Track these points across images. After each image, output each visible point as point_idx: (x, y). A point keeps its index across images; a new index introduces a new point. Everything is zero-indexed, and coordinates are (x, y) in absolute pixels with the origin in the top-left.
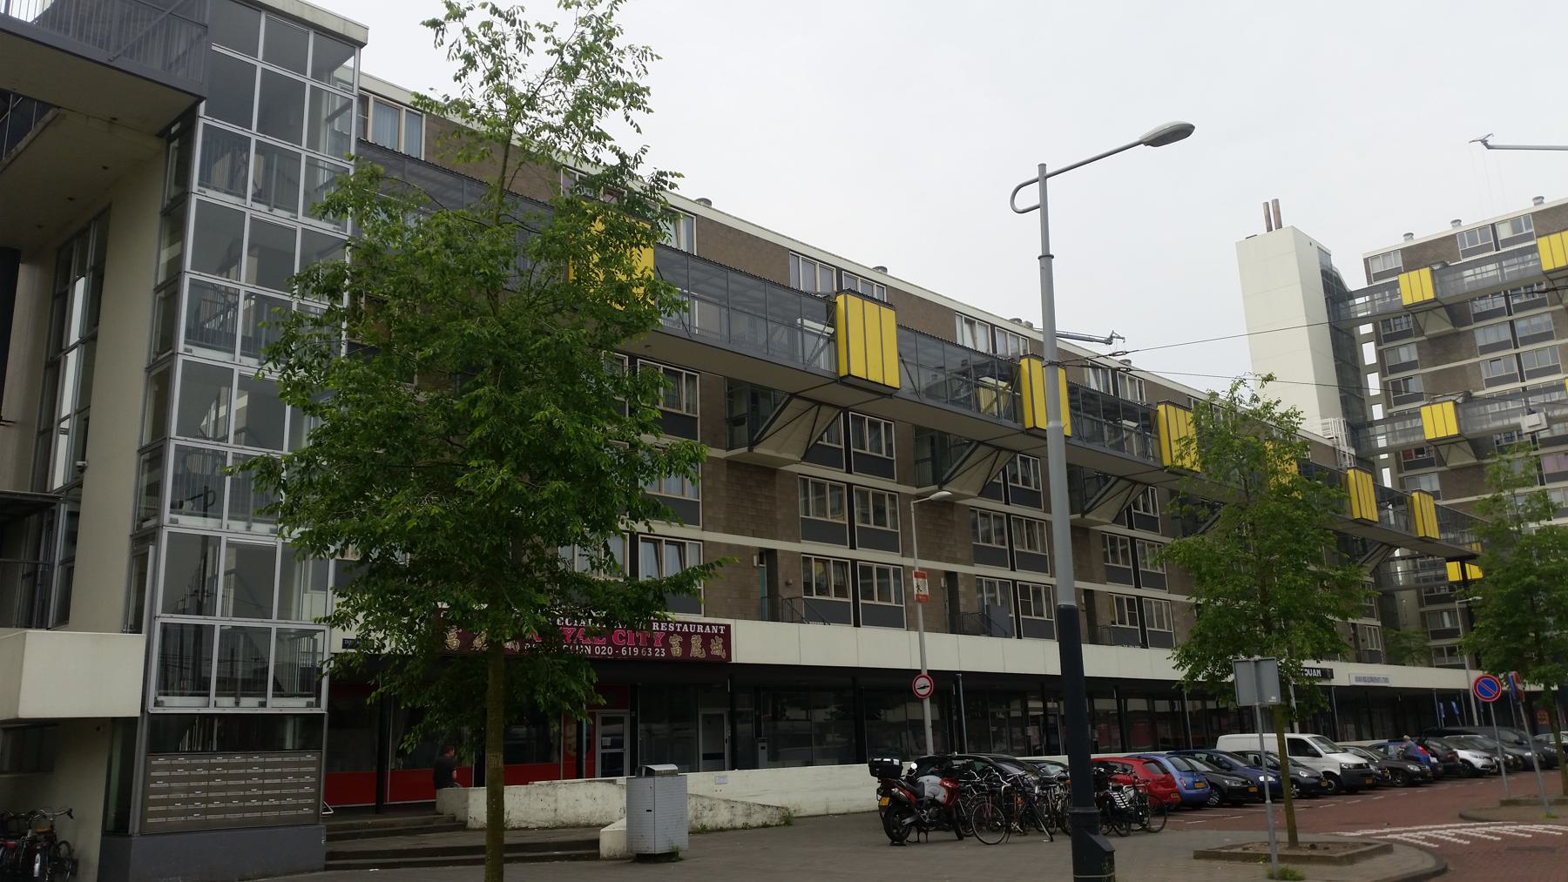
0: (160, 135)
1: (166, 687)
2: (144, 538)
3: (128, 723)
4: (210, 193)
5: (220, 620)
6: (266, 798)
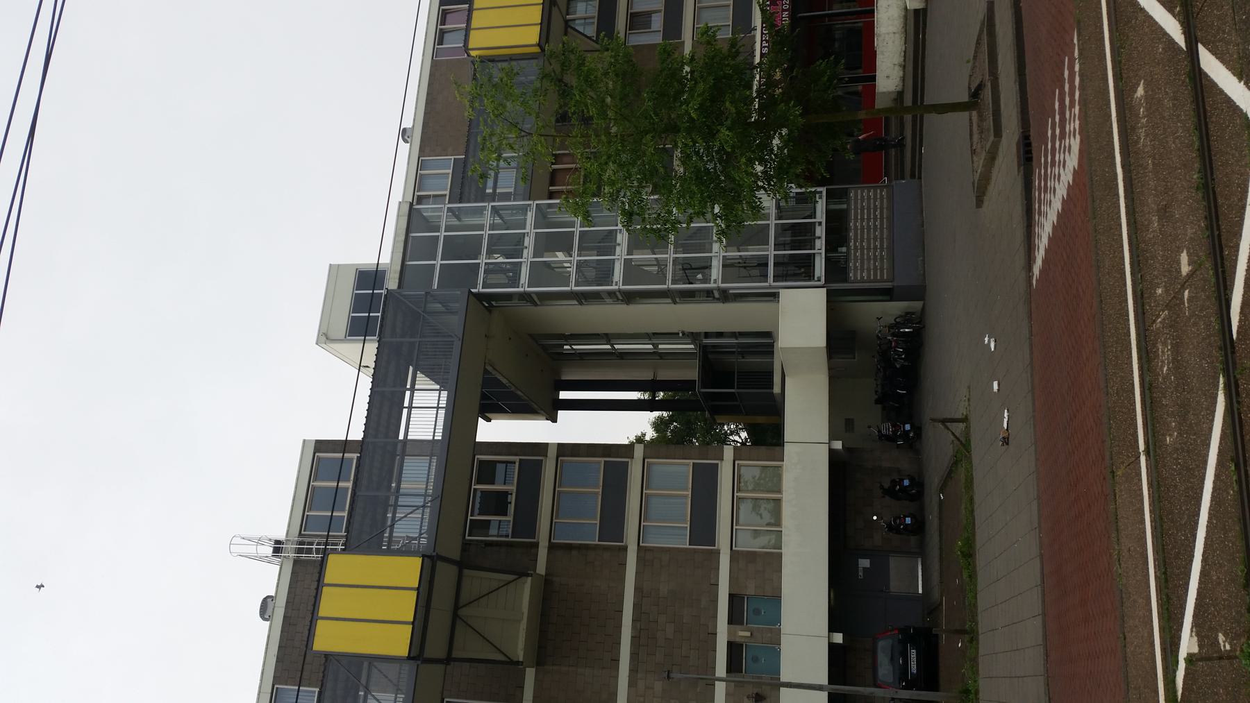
0: (490, 311)
1: (809, 275)
2: (725, 296)
3: (830, 294)
4: (522, 281)
5: (771, 252)
6: (875, 216)
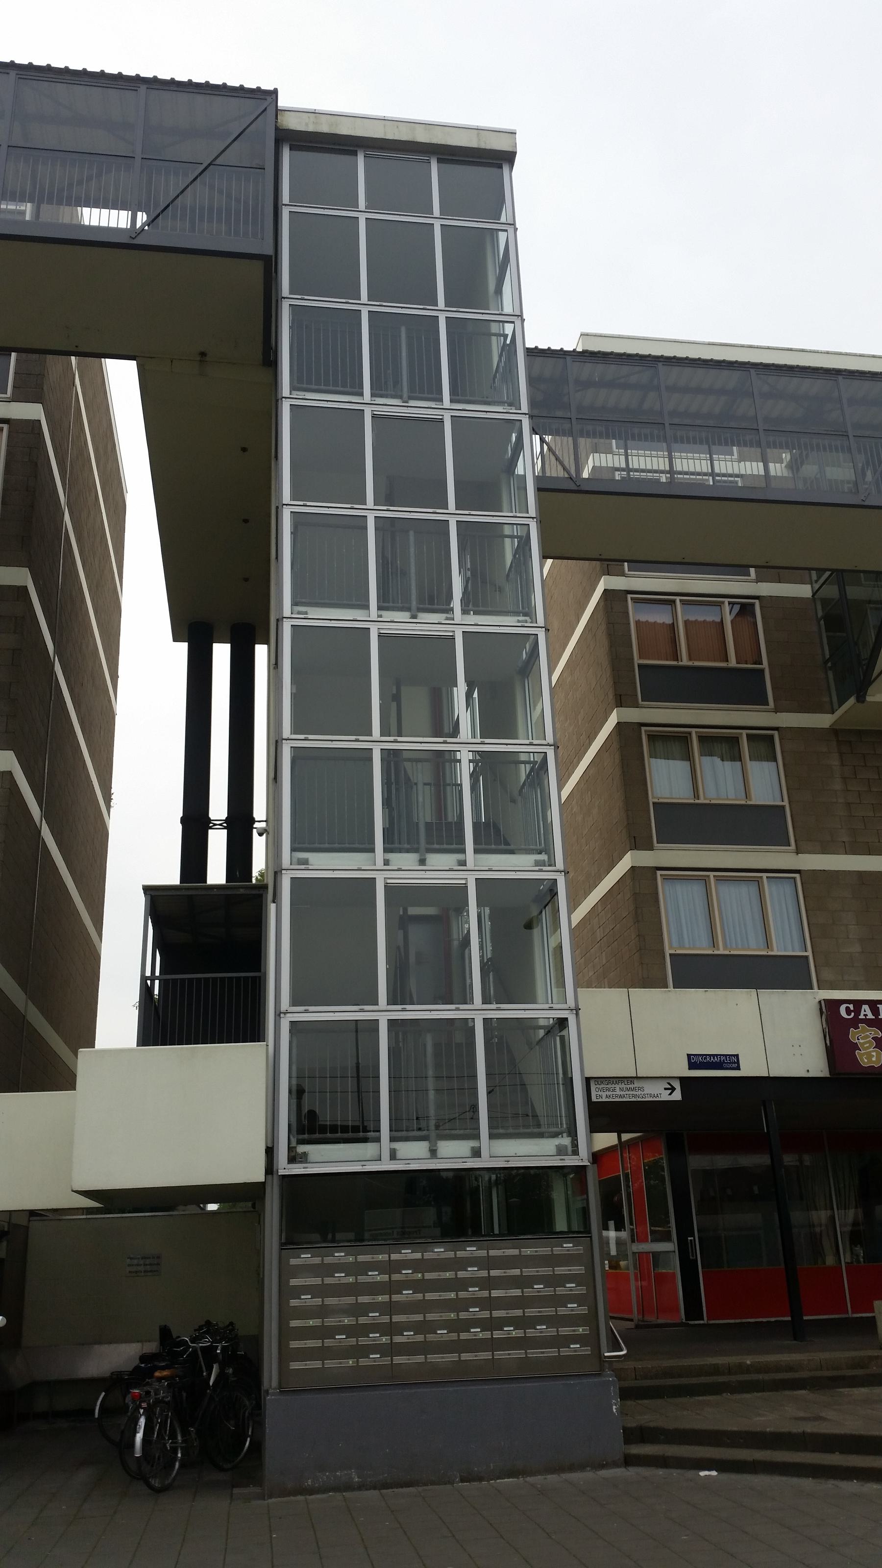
6: (499, 1324)
